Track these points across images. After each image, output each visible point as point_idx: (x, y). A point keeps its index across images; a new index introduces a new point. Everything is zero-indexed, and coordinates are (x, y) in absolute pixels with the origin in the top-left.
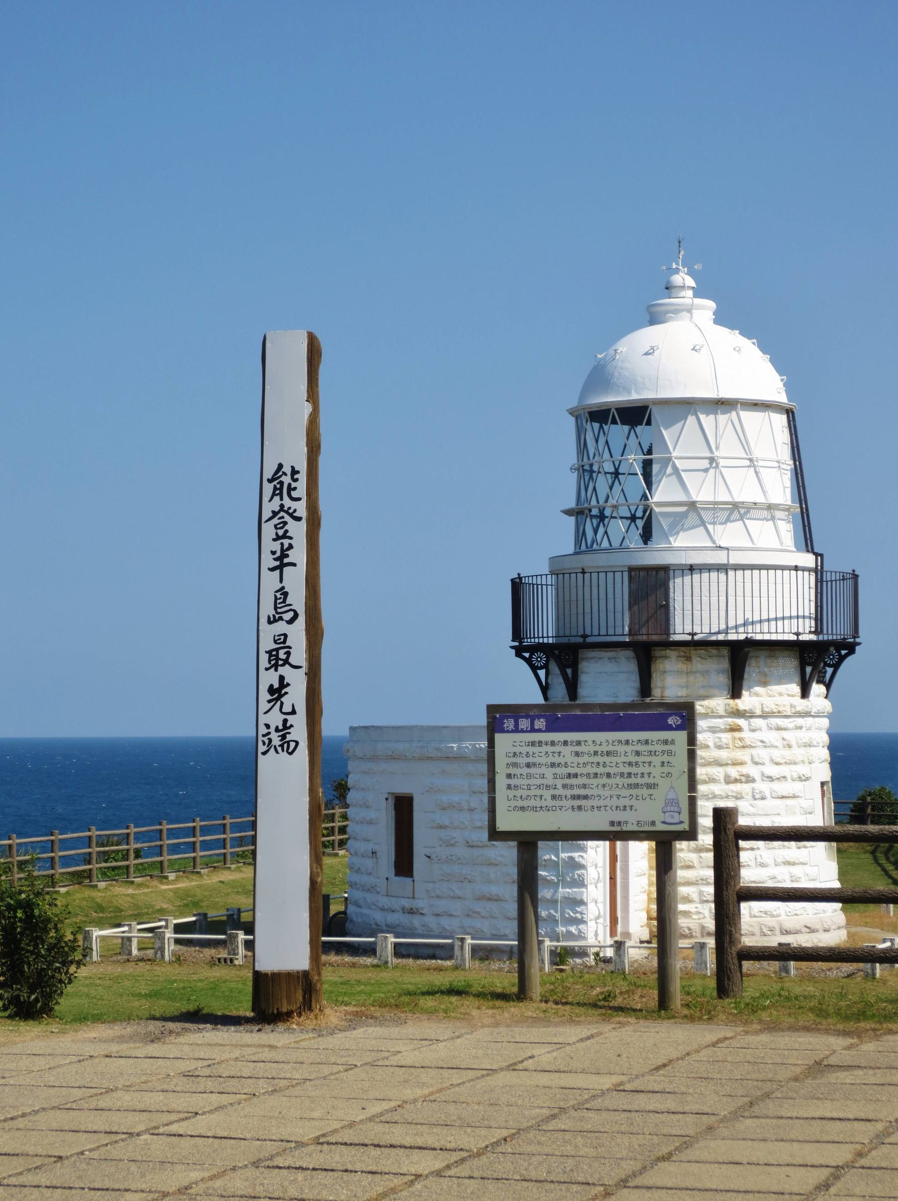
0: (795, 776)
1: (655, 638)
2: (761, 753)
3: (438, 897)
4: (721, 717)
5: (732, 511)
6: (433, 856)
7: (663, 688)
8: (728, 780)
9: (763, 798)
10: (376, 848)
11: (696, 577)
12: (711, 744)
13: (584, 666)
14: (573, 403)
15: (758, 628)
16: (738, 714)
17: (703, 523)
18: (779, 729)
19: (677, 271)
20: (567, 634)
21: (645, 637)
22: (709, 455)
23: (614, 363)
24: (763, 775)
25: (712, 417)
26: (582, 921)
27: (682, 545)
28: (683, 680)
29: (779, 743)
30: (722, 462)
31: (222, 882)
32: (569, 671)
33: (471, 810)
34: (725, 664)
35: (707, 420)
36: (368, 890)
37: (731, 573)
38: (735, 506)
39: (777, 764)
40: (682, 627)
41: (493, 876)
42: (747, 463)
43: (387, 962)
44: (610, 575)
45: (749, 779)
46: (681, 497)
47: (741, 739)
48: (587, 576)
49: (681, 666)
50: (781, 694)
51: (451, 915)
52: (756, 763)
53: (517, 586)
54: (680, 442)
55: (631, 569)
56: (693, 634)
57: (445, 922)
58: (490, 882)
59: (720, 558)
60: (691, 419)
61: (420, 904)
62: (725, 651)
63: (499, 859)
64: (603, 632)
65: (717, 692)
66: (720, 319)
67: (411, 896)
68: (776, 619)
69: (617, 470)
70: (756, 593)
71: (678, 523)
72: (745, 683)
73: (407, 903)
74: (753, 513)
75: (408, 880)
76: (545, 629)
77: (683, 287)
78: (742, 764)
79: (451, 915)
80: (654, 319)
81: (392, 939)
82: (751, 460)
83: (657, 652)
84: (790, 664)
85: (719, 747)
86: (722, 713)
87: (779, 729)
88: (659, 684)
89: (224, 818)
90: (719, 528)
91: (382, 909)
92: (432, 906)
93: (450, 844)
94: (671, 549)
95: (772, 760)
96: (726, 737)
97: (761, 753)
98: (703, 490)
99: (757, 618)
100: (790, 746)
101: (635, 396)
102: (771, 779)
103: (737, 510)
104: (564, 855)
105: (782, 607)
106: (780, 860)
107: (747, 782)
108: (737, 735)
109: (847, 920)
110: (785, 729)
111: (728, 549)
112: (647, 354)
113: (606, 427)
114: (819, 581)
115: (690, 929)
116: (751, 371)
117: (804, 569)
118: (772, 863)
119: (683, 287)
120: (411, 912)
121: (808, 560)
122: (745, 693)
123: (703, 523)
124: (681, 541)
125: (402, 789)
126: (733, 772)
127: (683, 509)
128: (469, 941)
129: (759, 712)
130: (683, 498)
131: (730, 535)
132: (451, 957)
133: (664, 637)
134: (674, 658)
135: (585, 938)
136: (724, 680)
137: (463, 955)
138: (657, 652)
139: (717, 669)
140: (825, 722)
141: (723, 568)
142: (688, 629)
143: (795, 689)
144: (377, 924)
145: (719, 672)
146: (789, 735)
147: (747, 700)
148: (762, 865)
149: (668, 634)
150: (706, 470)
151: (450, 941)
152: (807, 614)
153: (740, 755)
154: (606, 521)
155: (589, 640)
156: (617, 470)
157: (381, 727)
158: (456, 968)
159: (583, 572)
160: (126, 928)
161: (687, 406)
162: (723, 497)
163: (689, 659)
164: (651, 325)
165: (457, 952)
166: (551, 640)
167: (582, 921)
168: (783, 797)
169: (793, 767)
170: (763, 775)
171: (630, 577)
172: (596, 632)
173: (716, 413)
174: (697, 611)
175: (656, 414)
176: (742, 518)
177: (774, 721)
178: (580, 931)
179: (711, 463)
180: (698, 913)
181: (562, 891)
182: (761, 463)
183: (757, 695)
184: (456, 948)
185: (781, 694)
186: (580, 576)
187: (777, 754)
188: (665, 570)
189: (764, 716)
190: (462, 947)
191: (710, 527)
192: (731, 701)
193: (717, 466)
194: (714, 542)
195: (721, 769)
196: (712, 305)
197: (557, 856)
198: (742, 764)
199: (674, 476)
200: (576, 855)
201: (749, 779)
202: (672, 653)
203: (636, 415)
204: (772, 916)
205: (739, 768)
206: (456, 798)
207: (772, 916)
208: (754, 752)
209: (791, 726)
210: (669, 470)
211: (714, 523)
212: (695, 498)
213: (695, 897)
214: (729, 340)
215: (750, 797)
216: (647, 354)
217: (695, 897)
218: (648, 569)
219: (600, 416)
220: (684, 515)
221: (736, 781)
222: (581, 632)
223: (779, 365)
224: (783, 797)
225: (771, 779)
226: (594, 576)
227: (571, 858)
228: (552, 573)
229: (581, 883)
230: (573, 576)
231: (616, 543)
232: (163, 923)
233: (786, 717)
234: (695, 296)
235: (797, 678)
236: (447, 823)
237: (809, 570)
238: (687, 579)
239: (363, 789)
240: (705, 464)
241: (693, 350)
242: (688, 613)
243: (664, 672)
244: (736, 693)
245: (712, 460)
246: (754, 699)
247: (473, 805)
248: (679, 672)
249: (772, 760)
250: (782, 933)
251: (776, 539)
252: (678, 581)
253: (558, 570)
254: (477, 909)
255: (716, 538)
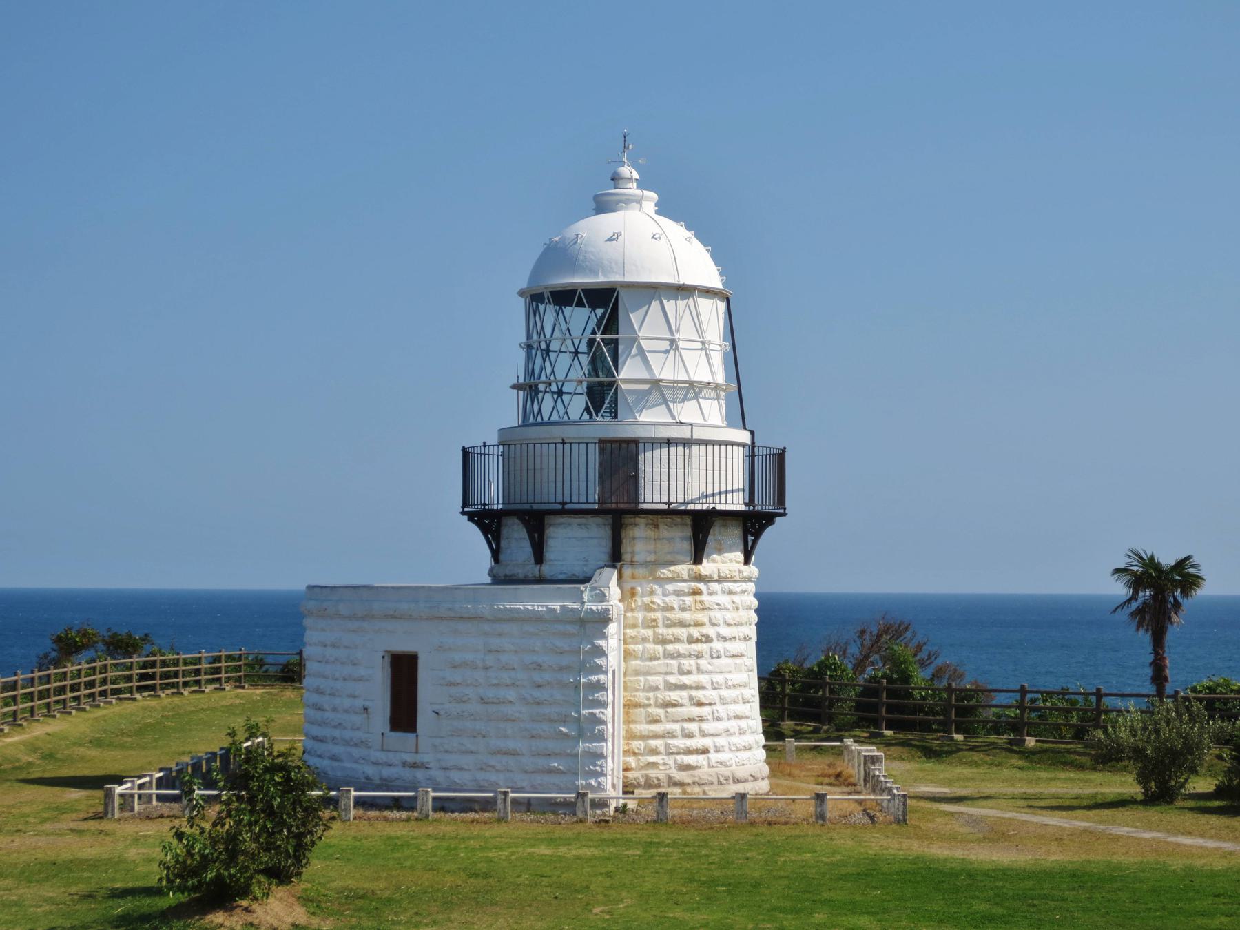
0: (742, 636)
1: (622, 506)
2: (717, 615)
3: (446, 751)
4: (685, 581)
5: (688, 390)
6: (442, 713)
7: (633, 553)
8: (691, 640)
9: (719, 657)
10: (367, 704)
11: (673, 449)
12: (676, 606)
13: (505, 532)
14: (524, 284)
15: (717, 499)
16: (700, 578)
17: (665, 402)
18: (730, 592)
19: (622, 164)
20: (531, 500)
21: (614, 506)
22: (669, 336)
23: (577, 247)
24: (718, 635)
25: (672, 302)
26: (603, 774)
27: (649, 420)
28: (651, 547)
29: (729, 606)
30: (682, 344)
31: (48, 734)
32: (751, 538)
33: (486, 668)
34: (688, 532)
35: (669, 305)
36: (356, 745)
37: (695, 448)
38: (691, 384)
39: (729, 625)
40: (652, 496)
41: (509, 732)
42: (699, 345)
43: (427, 816)
44: (583, 447)
45: (708, 639)
46: (645, 375)
47: (701, 602)
48: (567, 446)
49: (650, 533)
50: (731, 561)
51: (461, 769)
52: (714, 625)
53: (465, 452)
54: (645, 325)
55: (603, 442)
56: (669, 504)
57: (456, 776)
58: (506, 737)
59: (685, 433)
60: (655, 305)
61: (425, 758)
62: (688, 520)
63: (517, 715)
64: (583, 499)
65: (682, 558)
66: (663, 209)
67: (414, 749)
68: (726, 492)
69: (576, 350)
70: (723, 468)
71: (643, 399)
72: (707, 550)
73: (409, 758)
74: (705, 393)
75: (411, 736)
76: (493, 494)
77: (631, 179)
78: (702, 625)
79: (461, 769)
80: (602, 206)
81: (353, 793)
82: (703, 343)
83: (628, 519)
84: (734, 534)
85: (683, 609)
86: (686, 577)
87: (730, 592)
88: (629, 549)
89: (32, 672)
90: (680, 405)
91: (374, 763)
92: (439, 760)
93: (462, 701)
94: (637, 423)
95: (725, 622)
96: (689, 600)
97: (717, 615)
98: (665, 370)
99: (710, 492)
100: (737, 609)
101: (601, 279)
102: (725, 639)
103: (692, 389)
104: (584, 712)
105: (721, 481)
106: (732, 714)
107: (706, 642)
108: (698, 598)
109: (771, 770)
110: (734, 593)
111: (691, 425)
112: (610, 240)
113: (541, 307)
114: (752, 456)
115: (658, 779)
116: (694, 263)
117: (738, 444)
118: (725, 717)
119: (631, 179)
120: (414, 766)
121: (745, 437)
122: (705, 561)
123: (665, 402)
124: (645, 417)
125: (403, 646)
126: (695, 632)
127: (646, 387)
128: (353, 793)
129: (716, 578)
130: (646, 376)
131: (687, 412)
132: (413, 809)
133: (633, 505)
134: (642, 526)
135: (604, 790)
136: (687, 546)
137: (505, 807)
138: (549, 520)
139: (680, 537)
140: (751, 587)
141: (688, 443)
142: (665, 499)
143: (740, 556)
144: (367, 778)
145: (683, 539)
146: (736, 598)
147: (706, 567)
148: (718, 719)
149: (637, 503)
150: (667, 352)
151: (412, 794)
152: (741, 487)
153: (702, 617)
154: (540, 396)
155: (567, 507)
156: (576, 350)
157: (333, 588)
158: (499, 820)
159: (563, 443)
160: (129, 785)
161: (654, 291)
162: (682, 376)
163: (656, 526)
164: (598, 213)
165: (500, 805)
166: (500, 507)
167: (603, 774)
168: (734, 656)
169: (740, 628)
170: (718, 635)
171: (602, 451)
172: (575, 499)
173: (676, 299)
174: (663, 482)
175: (624, 299)
176: (696, 397)
177: (727, 585)
178: (599, 784)
179: (671, 345)
180: (665, 764)
181: (583, 746)
182: (712, 347)
183: (714, 561)
184: (499, 801)
185: (731, 561)
186: (560, 446)
187: (729, 615)
188: (635, 441)
189: (720, 580)
190: (505, 800)
191: (671, 405)
192: (694, 567)
193: (677, 348)
194: (674, 418)
195: (684, 630)
196: (655, 196)
197: (579, 712)
198: (702, 625)
199: (638, 358)
200: (596, 711)
201: (708, 639)
202: (641, 521)
203: (605, 300)
204: (726, 766)
205: (699, 629)
206: (469, 657)
207: (726, 766)
208: (712, 613)
209: (739, 590)
210: (634, 351)
211: (674, 402)
212: (657, 376)
213: (662, 749)
214: (676, 232)
215: (708, 656)
216: (610, 240)
217: (662, 749)
218: (620, 442)
219: (564, 297)
220: (649, 392)
221: (698, 641)
222: (559, 499)
223: (717, 258)
224: (734, 656)
225: (725, 639)
226: (575, 447)
227: (593, 714)
228: (501, 443)
229: (601, 738)
230: (552, 446)
231: (546, 419)
232: (147, 779)
233: (735, 581)
234: (638, 188)
235: (742, 547)
236: (459, 681)
237: (744, 445)
238: (665, 451)
239: (346, 647)
240: (666, 345)
241: (645, 240)
242: (657, 484)
243: (634, 538)
244: (697, 560)
245: (673, 342)
246: (711, 565)
247: (488, 663)
248: (648, 539)
249: (725, 622)
250: (734, 782)
251: (708, 416)
252: (648, 454)
253: (508, 440)
254: (492, 763)
255: (675, 414)
